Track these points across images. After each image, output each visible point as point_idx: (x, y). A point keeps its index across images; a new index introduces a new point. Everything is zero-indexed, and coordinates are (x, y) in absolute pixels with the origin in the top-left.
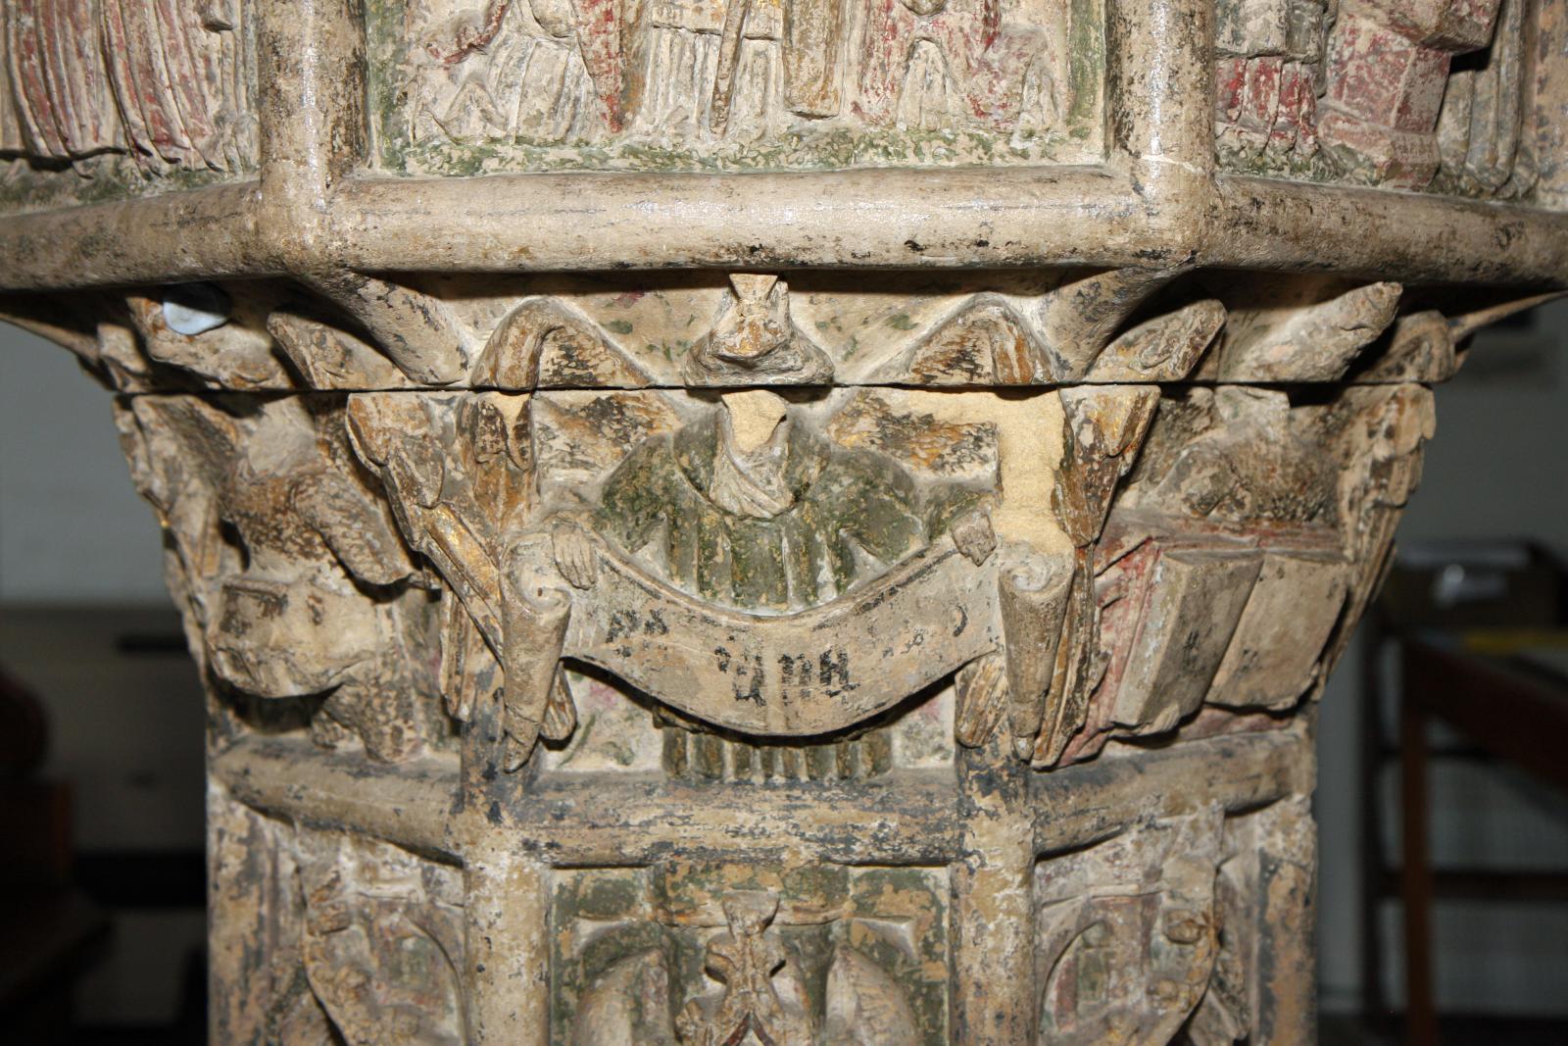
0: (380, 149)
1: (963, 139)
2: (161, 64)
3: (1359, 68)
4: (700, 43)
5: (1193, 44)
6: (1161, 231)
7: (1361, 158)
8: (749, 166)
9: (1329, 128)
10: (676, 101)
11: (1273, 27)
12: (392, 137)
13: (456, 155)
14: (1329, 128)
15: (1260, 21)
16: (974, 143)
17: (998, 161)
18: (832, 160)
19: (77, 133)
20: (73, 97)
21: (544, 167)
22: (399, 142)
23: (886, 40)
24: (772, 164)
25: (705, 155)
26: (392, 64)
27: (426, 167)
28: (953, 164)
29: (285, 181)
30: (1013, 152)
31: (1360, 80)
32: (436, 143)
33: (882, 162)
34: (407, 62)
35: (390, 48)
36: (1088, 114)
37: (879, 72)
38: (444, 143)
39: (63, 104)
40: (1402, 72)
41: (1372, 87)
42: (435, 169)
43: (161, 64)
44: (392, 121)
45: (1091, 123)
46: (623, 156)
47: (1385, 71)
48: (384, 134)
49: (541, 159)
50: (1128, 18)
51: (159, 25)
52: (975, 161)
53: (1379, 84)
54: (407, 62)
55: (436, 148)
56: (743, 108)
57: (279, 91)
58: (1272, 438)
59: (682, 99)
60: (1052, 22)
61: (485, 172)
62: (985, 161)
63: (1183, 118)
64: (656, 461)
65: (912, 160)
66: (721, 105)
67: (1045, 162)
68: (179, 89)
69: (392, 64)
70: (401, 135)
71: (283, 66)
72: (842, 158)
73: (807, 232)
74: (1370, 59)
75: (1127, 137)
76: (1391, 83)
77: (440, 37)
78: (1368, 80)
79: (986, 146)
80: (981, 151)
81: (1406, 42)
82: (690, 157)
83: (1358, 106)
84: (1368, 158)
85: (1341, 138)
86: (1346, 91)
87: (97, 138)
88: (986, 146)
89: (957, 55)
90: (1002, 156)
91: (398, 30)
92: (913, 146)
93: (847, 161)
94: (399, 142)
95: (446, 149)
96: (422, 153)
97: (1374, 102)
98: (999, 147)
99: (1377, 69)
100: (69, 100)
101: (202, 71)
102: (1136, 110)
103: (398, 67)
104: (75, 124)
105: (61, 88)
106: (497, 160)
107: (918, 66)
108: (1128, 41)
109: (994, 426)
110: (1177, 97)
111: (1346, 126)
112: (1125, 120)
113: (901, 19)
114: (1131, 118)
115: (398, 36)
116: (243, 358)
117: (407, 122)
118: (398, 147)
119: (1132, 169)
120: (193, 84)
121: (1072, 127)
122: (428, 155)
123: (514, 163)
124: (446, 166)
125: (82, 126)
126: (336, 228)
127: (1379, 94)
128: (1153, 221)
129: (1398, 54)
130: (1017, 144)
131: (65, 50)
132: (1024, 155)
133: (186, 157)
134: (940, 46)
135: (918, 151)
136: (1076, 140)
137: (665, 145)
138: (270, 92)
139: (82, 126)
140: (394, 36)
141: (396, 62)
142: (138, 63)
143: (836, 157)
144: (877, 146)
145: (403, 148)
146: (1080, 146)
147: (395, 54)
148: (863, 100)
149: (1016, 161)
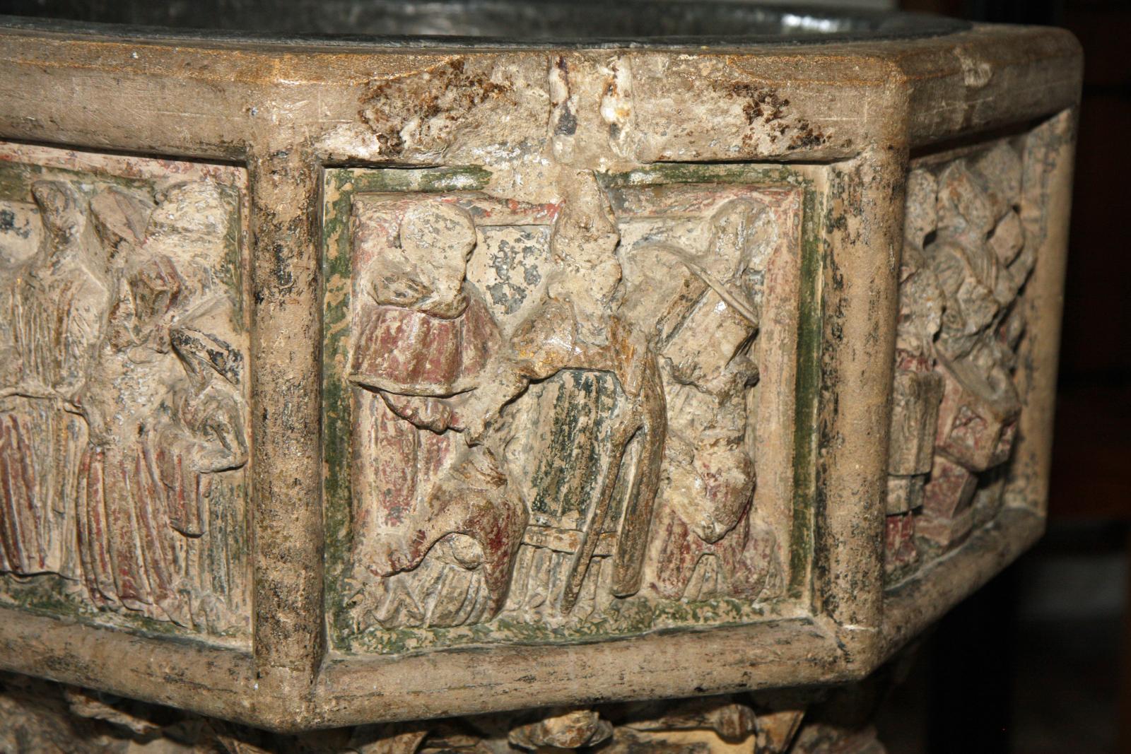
0: (331, 636)
1: (723, 605)
2: (139, 552)
4: (554, 555)
6: (853, 671)
7: (932, 543)
8: (586, 633)
10: (534, 590)
11: (902, 500)
12: (342, 628)
13: (386, 637)
16: (730, 608)
17: (745, 620)
18: (640, 626)
19: (26, 561)
20: (23, 536)
21: (448, 643)
22: (346, 631)
23: (682, 553)
24: (601, 632)
25: (555, 627)
26: (341, 578)
27: (365, 647)
28: (717, 623)
29: (281, 681)
30: (754, 612)
32: (371, 629)
33: (671, 624)
34: (352, 577)
35: (340, 567)
36: (801, 583)
37: (675, 572)
38: (376, 630)
39: (16, 543)
42: (372, 649)
43: (139, 552)
44: (341, 617)
45: (802, 589)
46: (499, 629)
48: (336, 626)
49: (445, 636)
50: (837, 537)
51: (139, 529)
52: (731, 620)
53: (945, 495)
54: (352, 577)
55: (371, 633)
56: (584, 604)
57: (278, 621)
59: (540, 590)
60: (779, 524)
61: (408, 649)
62: (737, 620)
65: (691, 622)
66: (570, 600)
67: (774, 617)
68: (151, 571)
69: (341, 578)
70: (348, 626)
71: (282, 605)
72: (646, 624)
73: (633, 687)
74: (941, 480)
75: (834, 611)
77: (376, 558)
79: (737, 609)
80: (734, 613)
81: (964, 471)
82: (546, 629)
84: (937, 543)
87: (42, 564)
88: (737, 609)
89: (728, 563)
90: (748, 615)
91: (346, 555)
92: (691, 612)
93: (649, 626)
94: (346, 631)
95: (379, 634)
96: (362, 638)
98: (746, 609)
99: (945, 486)
100: (20, 538)
101: (170, 557)
102: (841, 595)
103: (346, 580)
104: (24, 554)
105: (14, 531)
106: (415, 640)
107: (701, 570)
108: (836, 551)
109: (241, 150)
110: (867, 589)
112: (832, 599)
113: (694, 542)
114: (837, 600)
115: (346, 559)
117: (353, 618)
118: (345, 635)
119: (837, 632)
120: (162, 564)
122: (366, 639)
123: (427, 641)
124: (380, 646)
125: (29, 558)
126: (318, 710)
127: (944, 501)
128: (850, 666)
129: (958, 477)
130: (756, 606)
131: (19, 504)
132: (761, 612)
133: (149, 611)
134: (718, 558)
135: (695, 617)
136: (793, 600)
137: (528, 620)
138: (270, 620)
139: (29, 558)
140: (343, 559)
141: (345, 577)
142: (118, 550)
143: (642, 623)
144: (668, 613)
145: (349, 635)
146: (795, 604)
147: (343, 571)
148: (660, 585)
149: (757, 618)
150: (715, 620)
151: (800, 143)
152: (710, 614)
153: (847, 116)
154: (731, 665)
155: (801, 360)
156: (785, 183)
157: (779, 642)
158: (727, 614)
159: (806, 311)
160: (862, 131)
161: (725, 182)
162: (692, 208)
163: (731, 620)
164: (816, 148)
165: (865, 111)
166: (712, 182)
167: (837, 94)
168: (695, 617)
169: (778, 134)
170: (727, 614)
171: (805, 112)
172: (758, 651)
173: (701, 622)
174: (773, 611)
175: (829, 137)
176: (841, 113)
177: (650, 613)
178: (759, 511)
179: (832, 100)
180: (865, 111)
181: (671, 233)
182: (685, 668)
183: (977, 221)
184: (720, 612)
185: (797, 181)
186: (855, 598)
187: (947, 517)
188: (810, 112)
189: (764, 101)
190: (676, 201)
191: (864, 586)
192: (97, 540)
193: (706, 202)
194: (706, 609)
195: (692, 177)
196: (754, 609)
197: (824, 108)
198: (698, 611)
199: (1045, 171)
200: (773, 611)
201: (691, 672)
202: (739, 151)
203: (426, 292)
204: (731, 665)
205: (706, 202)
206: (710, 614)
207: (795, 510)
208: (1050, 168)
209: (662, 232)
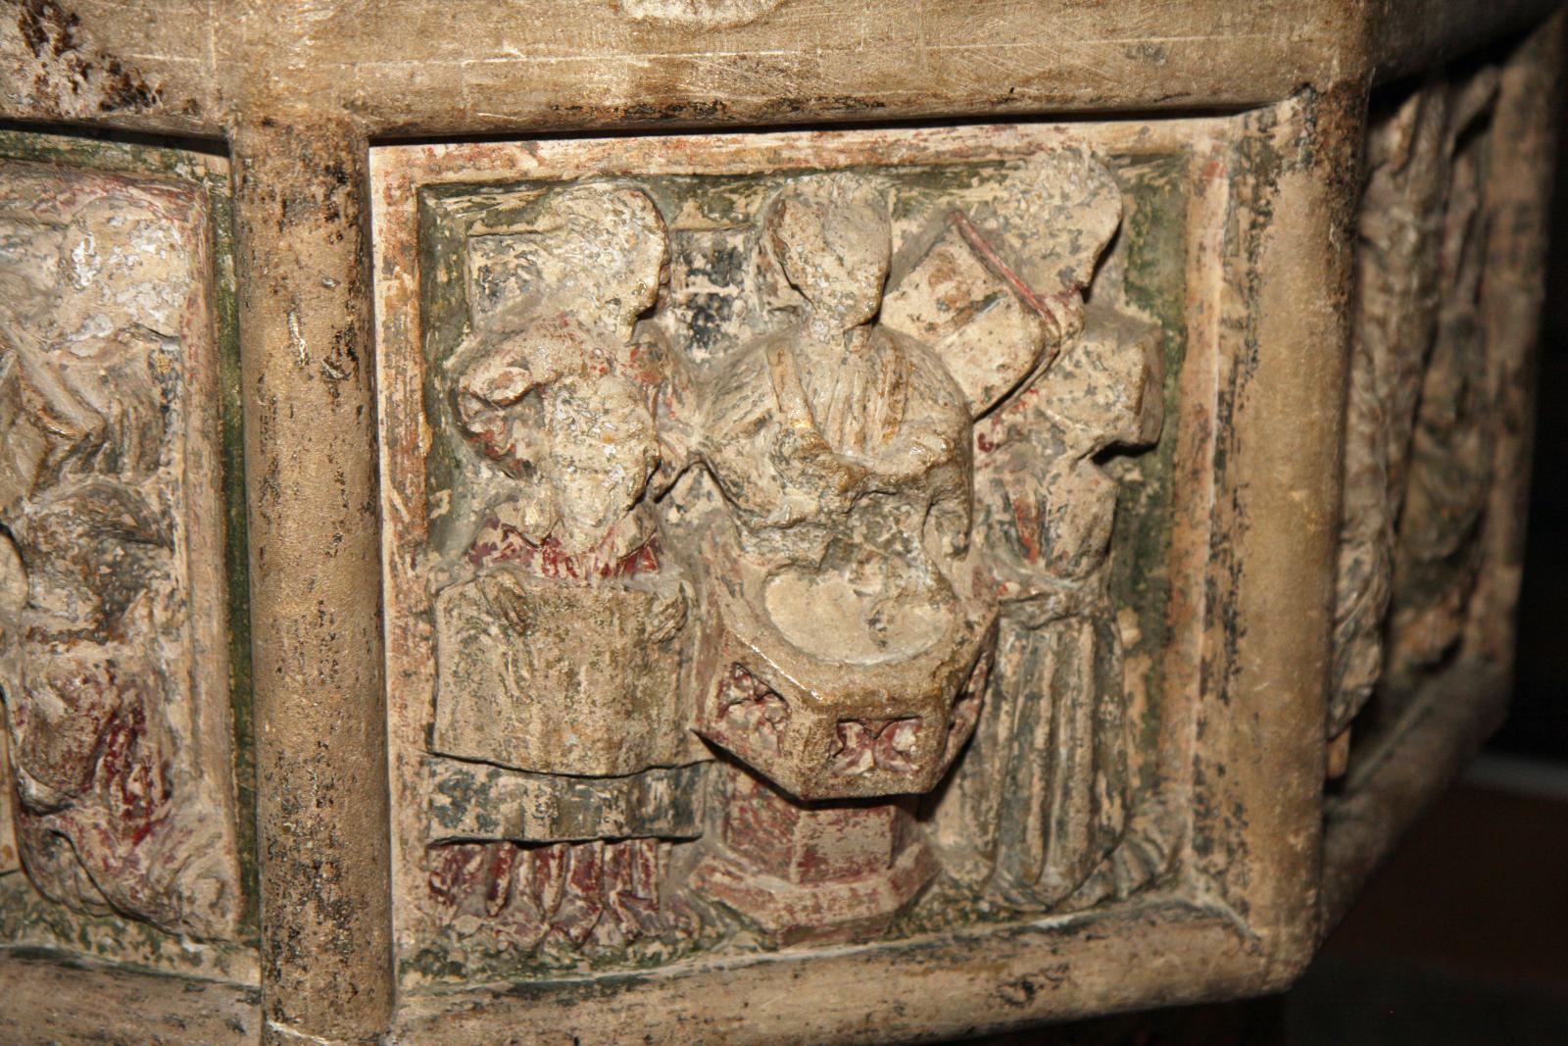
3: (742, 810)
5: (320, 900)
9: (704, 881)
14: (704, 881)
15: (515, 805)
17: (164, 967)
28: (117, 960)
31: (747, 825)
40: (795, 824)
41: (760, 834)
47: (775, 819)
58: (1440, 641)
62: (151, 963)
63: (308, 985)
64: (1321, 139)
76: (783, 834)
78: (756, 826)
80: (147, 950)
83: (745, 853)
85: (718, 894)
86: (730, 834)
90: (170, 960)
97: (767, 852)
111: (727, 880)
116: (36, 727)
121: (244, 938)
132: (195, 960)
149: (184, 969)
150: (115, 954)
151: (117, 100)
152: (109, 941)
153: (179, 53)
154: (83, 1037)
155: (233, 512)
156: (170, 174)
157: (167, 1020)
158: (136, 947)
159: (236, 422)
160: (211, 85)
161: (69, 163)
162: (43, 206)
163: (141, 961)
164: (145, 111)
165: (212, 47)
166: (47, 161)
167: (159, 9)
168: (84, 938)
169: (79, 78)
170: (136, 947)
171: (107, 40)
172: (128, 1026)
173: (94, 951)
174: (218, 963)
175: (160, 92)
176: (169, 49)
177: (21, 915)
178: (206, 777)
179: (151, 20)
180: (212, 47)
181: (31, 250)
182: (12, 1023)
183: (833, 302)
184: (126, 940)
185: (193, 173)
186: (279, 974)
187: (786, 877)
188: (115, 42)
189: (42, 14)
190: (12, 191)
191: (294, 956)
192: (908, 707)
193: (61, 197)
194: (104, 930)
195: (15, 148)
196: (185, 950)
197: (139, 35)
198: (90, 930)
199: (1254, 225)
200: (218, 963)
201: (20, 1032)
202: (34, 108)
203: (351, 328)
204: (83, 1037)
205: (61, 197)
206: (109, 941)
207: (241, 789)
208: (1261, 219)
209: (14, 245)
